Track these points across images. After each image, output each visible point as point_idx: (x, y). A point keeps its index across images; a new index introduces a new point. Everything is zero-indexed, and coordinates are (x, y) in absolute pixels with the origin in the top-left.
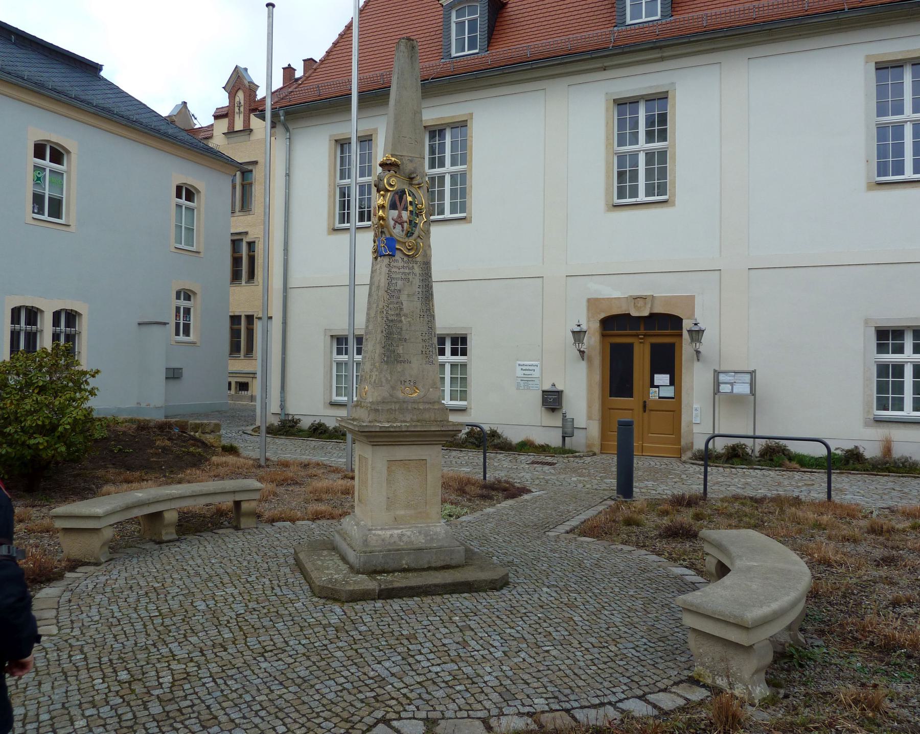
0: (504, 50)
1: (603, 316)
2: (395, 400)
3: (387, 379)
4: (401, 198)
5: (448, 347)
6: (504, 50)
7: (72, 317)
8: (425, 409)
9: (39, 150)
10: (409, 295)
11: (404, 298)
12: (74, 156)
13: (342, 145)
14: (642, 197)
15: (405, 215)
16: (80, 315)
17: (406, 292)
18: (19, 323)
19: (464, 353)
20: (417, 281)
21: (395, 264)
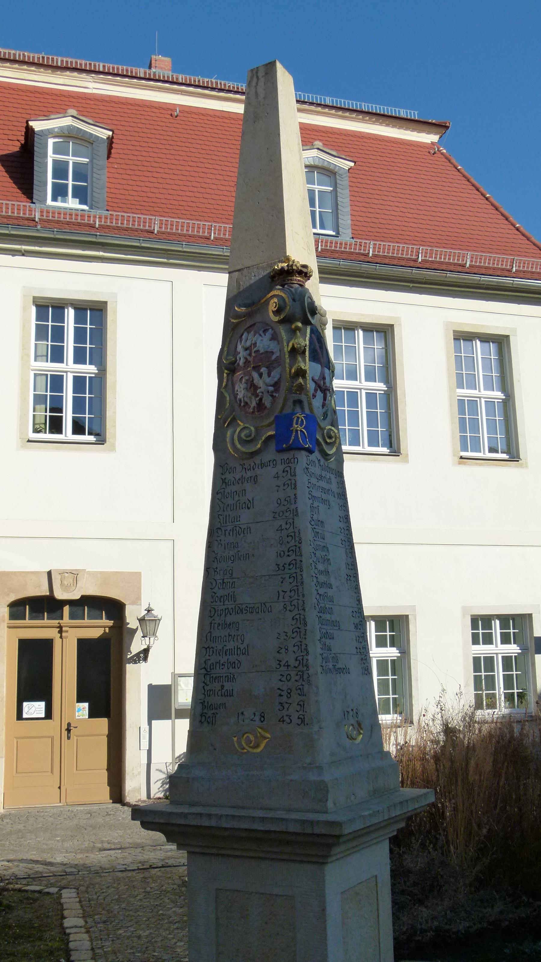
1: (13, 598)
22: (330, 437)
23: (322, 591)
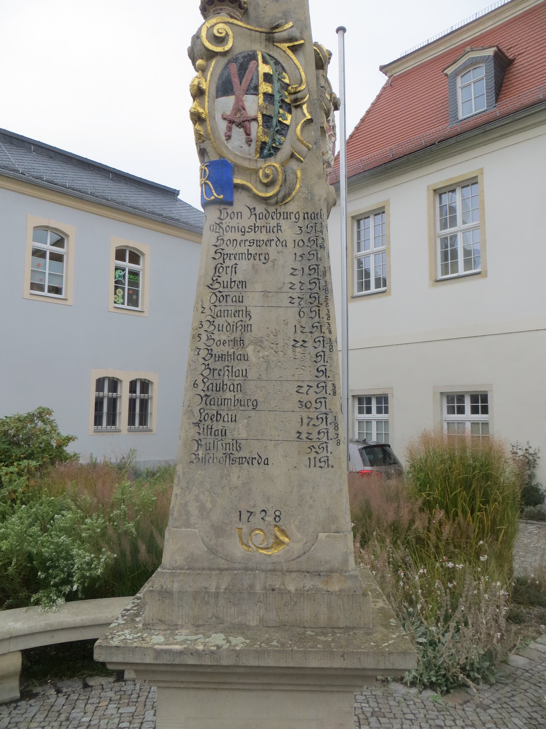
0: (511, 102)
2: (222, 563)
3: (202, 508)
4: (243, 69)
5: (468, 404)
6: (511, 102)
7: (145, 385)
8: (301, 593)
9: (120, 254)
10: (265, 293)
11: (252, 300)
12: (147, 257)
13: (358, 221)
14: (373, 289)
15: (253, 105)
16: (152, 383)
17: (259, 287)
18: (103, 391)
19: (485, 410)
20: (286, 259)
21: (234, 222)
22: (267, 176)
23: (218, 365)
